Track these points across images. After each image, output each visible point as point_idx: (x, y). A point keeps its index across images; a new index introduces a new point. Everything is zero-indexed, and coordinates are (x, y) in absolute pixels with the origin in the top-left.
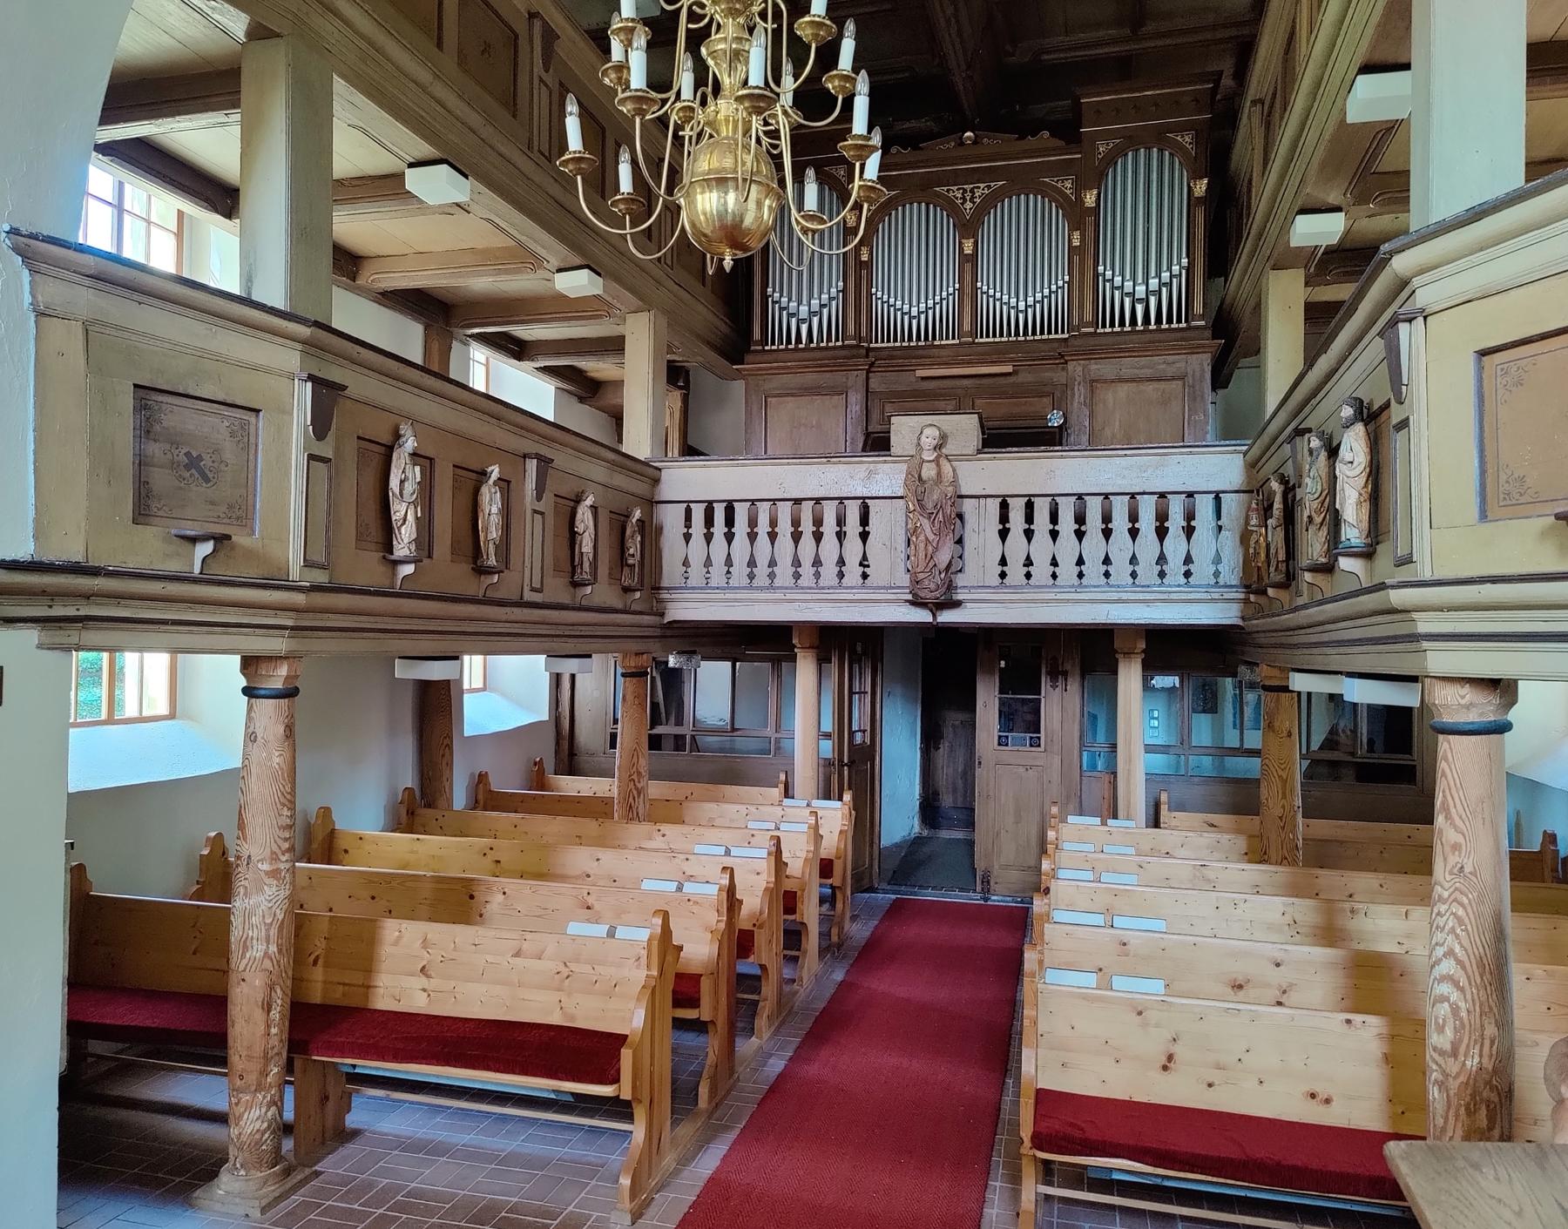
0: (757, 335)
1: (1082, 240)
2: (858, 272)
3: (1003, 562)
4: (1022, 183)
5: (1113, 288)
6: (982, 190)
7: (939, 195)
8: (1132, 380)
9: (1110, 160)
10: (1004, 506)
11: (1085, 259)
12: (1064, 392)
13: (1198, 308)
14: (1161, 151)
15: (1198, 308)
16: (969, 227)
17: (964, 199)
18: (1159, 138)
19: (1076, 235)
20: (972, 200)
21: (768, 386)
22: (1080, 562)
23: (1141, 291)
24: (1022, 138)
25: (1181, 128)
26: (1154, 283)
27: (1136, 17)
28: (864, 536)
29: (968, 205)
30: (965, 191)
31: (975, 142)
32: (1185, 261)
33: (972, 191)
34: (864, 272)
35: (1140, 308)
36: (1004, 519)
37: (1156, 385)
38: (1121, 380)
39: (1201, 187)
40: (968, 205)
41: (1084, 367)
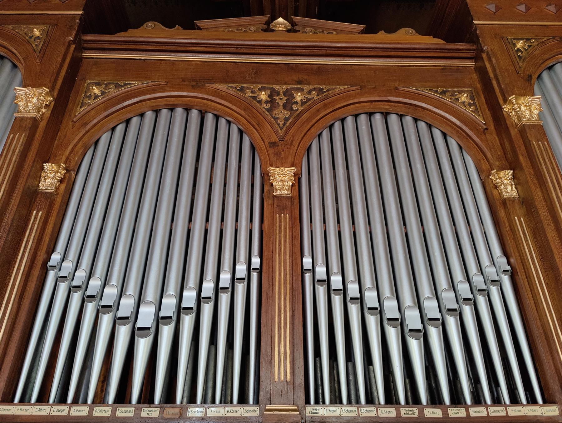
24: (370, 30)
29: (281, 114)
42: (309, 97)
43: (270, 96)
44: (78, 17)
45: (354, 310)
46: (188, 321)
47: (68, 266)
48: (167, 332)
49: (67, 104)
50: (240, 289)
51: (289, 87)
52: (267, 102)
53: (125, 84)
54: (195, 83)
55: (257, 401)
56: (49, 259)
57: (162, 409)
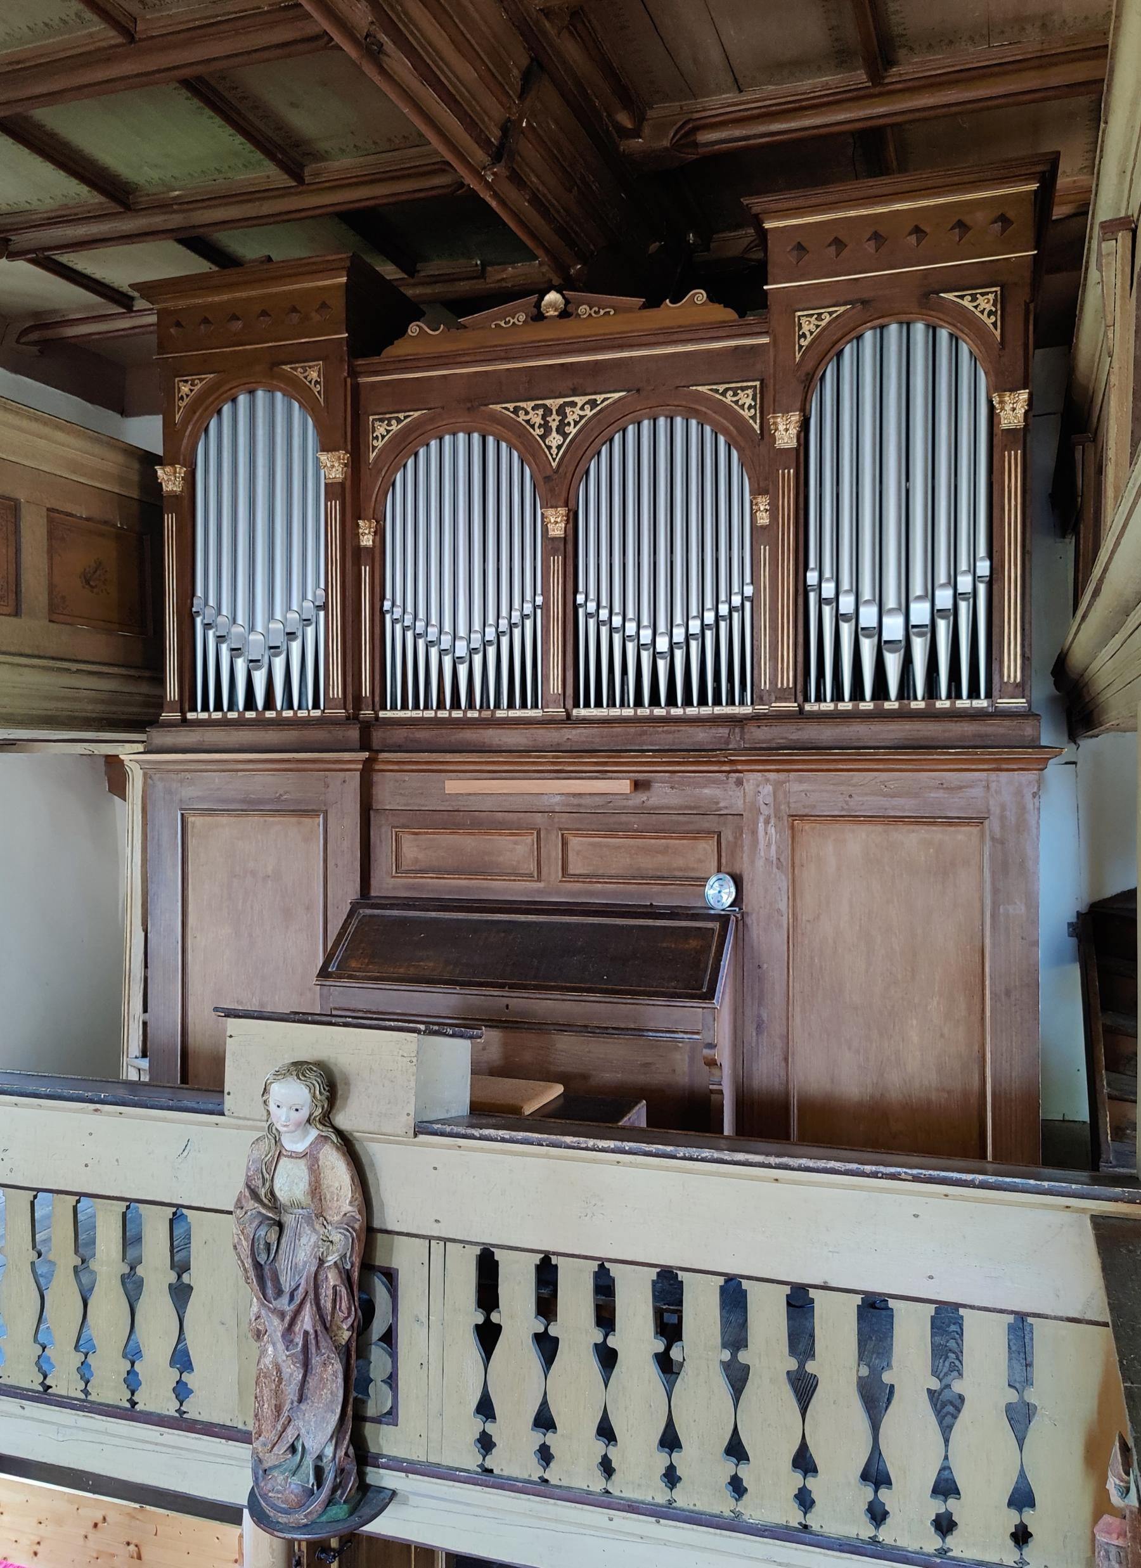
0: (172, 690)
1: (773, 511)
2: (358, 570)
3: (485, 1408)
4: (656, 392)
5: (838, 617)
6: (580, 409)
7: (497, 419)
8: (871, 819)
9: (829, 348)
10: (487, 1268)
11: (793, 539)
12: (739, 831)
13: (1012, 669)
14: (933, 329)
15: (1012, 669)
16: (559, 485)
17: (546, 426)
18: (927, 300)
19: (763, 502)
20: (560, 430)
21: (188, 792)
22: (670, 1441)
23: (894, 628)
24: (653, 302)
25: (302, 356)
26: (920, 612)
27: (878, 49)
28: (181, 1294)
29: (555, 439)
30: (547, 411)
31: (564, 314)
32: (983, 568)
33: (561, 411)
34: (366, 571)
35: (893, 663)
36: (488, 1293)
37: (923, 832)
38: (855, 819)
39: (1014, 410)
40: (555, 439)
41: (777, 785)
42: (582, 413)
43: (544, 417)
44: (345, 343)
45: (617, 638)
46: (491, 651)
47: (398, 612)
48: (477, 659)
49: (359, 448)
50: (528, 623)
51: (561, 401)
52: (540, 426)
53: (406, 417)
54: (469, 405)
55: (989, 695)
56: (382, 606)
57: (480, 712)
